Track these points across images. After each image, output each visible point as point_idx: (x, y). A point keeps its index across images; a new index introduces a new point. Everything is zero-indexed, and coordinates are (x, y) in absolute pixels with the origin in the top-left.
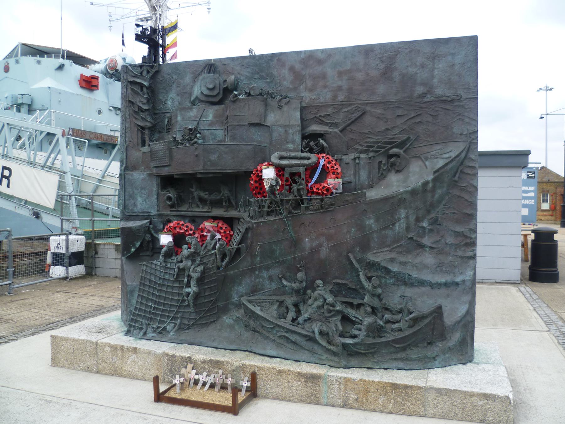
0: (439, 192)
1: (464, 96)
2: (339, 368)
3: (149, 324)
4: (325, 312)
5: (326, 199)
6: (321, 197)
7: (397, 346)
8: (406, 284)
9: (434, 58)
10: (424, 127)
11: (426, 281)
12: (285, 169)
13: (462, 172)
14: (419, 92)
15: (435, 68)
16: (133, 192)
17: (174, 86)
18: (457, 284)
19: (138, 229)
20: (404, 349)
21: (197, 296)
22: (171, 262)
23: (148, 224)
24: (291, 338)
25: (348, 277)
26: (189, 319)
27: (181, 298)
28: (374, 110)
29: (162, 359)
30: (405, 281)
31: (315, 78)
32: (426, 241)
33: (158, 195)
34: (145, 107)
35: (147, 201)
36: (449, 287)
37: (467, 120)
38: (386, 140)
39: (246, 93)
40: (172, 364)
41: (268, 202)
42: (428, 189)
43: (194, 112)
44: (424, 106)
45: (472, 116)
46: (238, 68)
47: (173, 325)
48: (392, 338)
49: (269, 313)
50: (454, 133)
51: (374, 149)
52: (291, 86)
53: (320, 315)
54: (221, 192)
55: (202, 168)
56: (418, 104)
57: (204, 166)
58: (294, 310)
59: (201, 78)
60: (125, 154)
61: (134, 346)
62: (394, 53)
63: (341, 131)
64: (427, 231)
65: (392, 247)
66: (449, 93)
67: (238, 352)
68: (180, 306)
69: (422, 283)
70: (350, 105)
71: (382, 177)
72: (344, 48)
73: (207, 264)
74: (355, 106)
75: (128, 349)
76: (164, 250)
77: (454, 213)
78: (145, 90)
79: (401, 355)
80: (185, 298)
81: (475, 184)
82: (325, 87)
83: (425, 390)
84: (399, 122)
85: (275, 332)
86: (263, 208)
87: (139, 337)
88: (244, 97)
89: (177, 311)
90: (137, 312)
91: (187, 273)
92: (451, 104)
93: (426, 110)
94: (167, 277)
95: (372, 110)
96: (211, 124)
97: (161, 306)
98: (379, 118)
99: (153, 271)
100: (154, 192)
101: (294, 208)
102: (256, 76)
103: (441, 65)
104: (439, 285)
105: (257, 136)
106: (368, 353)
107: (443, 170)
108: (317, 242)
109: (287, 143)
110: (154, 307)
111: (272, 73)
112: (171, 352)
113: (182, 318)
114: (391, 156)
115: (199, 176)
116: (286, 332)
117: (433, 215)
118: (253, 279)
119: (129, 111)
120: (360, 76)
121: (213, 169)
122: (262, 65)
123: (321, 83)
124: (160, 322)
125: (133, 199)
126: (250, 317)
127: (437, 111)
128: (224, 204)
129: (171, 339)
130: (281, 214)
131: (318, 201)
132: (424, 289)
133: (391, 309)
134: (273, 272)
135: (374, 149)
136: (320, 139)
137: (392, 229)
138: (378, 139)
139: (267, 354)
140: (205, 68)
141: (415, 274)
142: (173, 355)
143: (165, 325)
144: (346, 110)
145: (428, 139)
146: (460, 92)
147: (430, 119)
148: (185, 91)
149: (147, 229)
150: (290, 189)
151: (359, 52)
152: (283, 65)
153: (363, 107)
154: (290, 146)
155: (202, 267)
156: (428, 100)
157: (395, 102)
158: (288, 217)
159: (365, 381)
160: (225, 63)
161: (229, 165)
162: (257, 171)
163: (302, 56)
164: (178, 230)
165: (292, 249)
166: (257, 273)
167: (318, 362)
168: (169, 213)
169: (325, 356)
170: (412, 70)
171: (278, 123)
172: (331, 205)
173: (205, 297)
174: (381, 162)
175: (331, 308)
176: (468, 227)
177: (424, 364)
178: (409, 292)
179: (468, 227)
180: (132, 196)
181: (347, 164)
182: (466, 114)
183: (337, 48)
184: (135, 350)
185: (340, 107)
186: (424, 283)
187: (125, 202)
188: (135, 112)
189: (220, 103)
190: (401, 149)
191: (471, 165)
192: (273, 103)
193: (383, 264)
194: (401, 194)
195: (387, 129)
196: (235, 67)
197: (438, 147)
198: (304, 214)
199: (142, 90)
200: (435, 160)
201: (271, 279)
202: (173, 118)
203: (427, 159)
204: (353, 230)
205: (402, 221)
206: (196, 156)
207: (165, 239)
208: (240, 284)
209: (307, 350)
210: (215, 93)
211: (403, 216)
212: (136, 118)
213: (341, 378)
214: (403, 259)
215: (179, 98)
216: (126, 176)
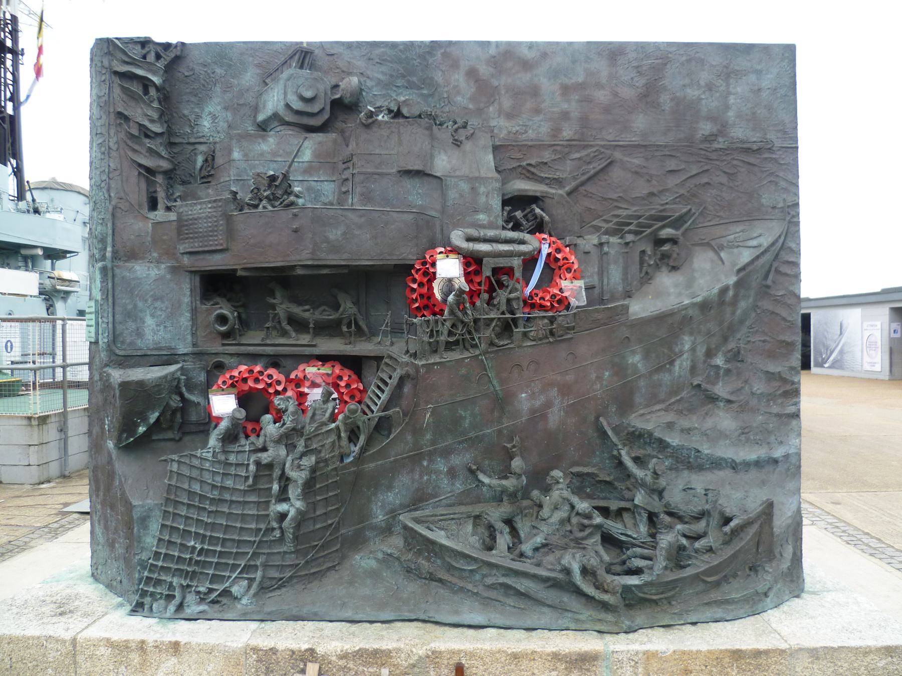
0: (743, 305)
1: (778, 144)
2: (617, 633)
3: (188, 586)
4: (575, 529)
5: (561, 318)
6: (550, 314)
7: (709, 579)
8: (690, 467)
9: (728, 76)
10: (714, 192)
11: (725, 460)
12: (485, 260)
13: (777, 272)
14: (703, 132)
15: (729, 93)
16: (135, 306)
17: (218, 89)
18: (776, 461)
19: (158, 385)
20: (717, 584)
21: (302, 519)
22: (238, 452)
23: (179, 373)
24: (518, 586)
25: (596, 460)
26: (281, 568)
27: (263, 526)
28: (628, 159)
29: (243, 660)
30: (689, 462)
31: (517, 93)
32: (721, 389)
33: (194, 311)
34: (157, 128)
35: (168, 324)
36: (763, 467)
37: (783, 184)
38: (653, 212)
39: (390, 111)
40: (267, 668)
41: (448, 324)
42: (727, 299)
43: (269, 144)
44: (713, 156)
45: (790, 177)
46: (360, 64)
47: (245, 583)
48: (704, 567)
49: (464, 539)
50: (763, 205)
51: (631, 227)
52: (471, 106)
53: (565, 536)
54: (339, 306)
55: (309, 256)
56: (703, 152)
57: (313, 253)
58: (508, 530)
59: (285, 75)
60: (110, 225)
61: (173, 639)
62: (660, 61)
63: (569, 194)
64: (722, 372)
65: (668, 403)
66: (755, 137)
67: (399, 624)
68: (260, 542)
69: (717, 464)
70: (585, 147)
71: (647, 278)
72: (571, 44)
73: (320, 452)
74: (594, 149)
75: (157, 647)
76: (223, 425)
77: (764, 341)
78: (153, 92)
79: (715, 595)
80: (275, 525)
81: (796, 291)
82: (537, 111)
83: (791, 654)
84: (672, 181)
85: (478, 577)
86: (438, 335)
87: (168, 615)
88: (386, 118)
89: (254, 554)
90: (160, 564)
91: (277, 473)
92: (758, 156)
93: (718, 163)
94: (229, 483)
95: (626, 159)
96: (309, 169)
97: (217, 545)
98: (636, 173)
99: (195, 473)
100: (184, 306)
101: (499, 336)
102: (400, 82)
103: (740, 88)
104: (747, 465)
105: (417, 194)
106: (661, 599)
107: (751, 267)
108: (542, 398)
109: (476, 211)
110: (202, 549)
111: (432, 79)
112: (264, 643)
113: (265, 566)
114: (662, 244)
115: (300, 272)
116: (503, 575)
117: (732, 345)
118: (417, 477)
119: (117, 132)
120: (602, 96)
121: (334, 259)
122: (414, 62)
123: (529, 105)
124: (215, 579)
125: (135, 321)
126: (419, 553)
127: (735, 166)
128: (345, 329)
129: (245, 614)
130: (475, 346)
131: (546, 321)
132: (721, 474)
133: (681, 513)
134: (457, 460)
135: (631, 227)
136: (534, 206)
137: (669, 371)
138: (635, 211)
139: (466, 623)
140: (291, 57)
141: (706, 450)
142: (271, 649)
143: (227, 584)
144: (577, 155)
145: (721, 214)
146: (771, 136)
147: (724, 179)
148: (241, 102)
149: (175, 383)
150: (491, 298)
151: (599, 54)
152: (455, 65)
153: (608, 152)
154: (482, 217)
155: (313, 459)
156: (720, 146)
157: (666, 146)
158: (488, 352)
159: (684, 652)
160: (332, 52)
161: (365, 248)
162: (424, 263)
163: (492, 51)
164: (251, 383)
165: (496, 414)
166: (425, 463)
167: (573, 626)
168: (221, 349)
169: (586, 613)
170: (692, 93)
171: (458, 173)
172: (568, 328)
173: (315, 520)
174: (643, 252)
175: (586, 522)
176: (787, 364)
177: (752, 607)
178: (699, 481)
179: (787, 364)
180: (132, 315)
181: (587, 253)
182: (781, 174)
183: (557, 43)
184: (176, 647)
185: (567, 150)
186: (720, 464)
187: (114, 327)
188: (132, 136)
189: (322, 128)
190: (677, 229)
191: (791, 260)
192: (444, 135)
193: (657, 434)
194: (686, 309)
195: (652, 194)
196: (354, 61)
197: (739, 228)
198: (520, 347)
199: (146, 92)
200: (735, 250)
201: (452, 473)
202: (218, 154)
203: (721, 247)
204: (607, 373)
205: (685, 356)
206: (296, 231)
207: (223, 405)
208: (390, 488)
209: (549, 606)
210: (316, 108)
211: (687, 347)
212: (134, 151)
213: (637, 653)
214: (685, 423)
215: (229, 114)
216: (117, 271)
